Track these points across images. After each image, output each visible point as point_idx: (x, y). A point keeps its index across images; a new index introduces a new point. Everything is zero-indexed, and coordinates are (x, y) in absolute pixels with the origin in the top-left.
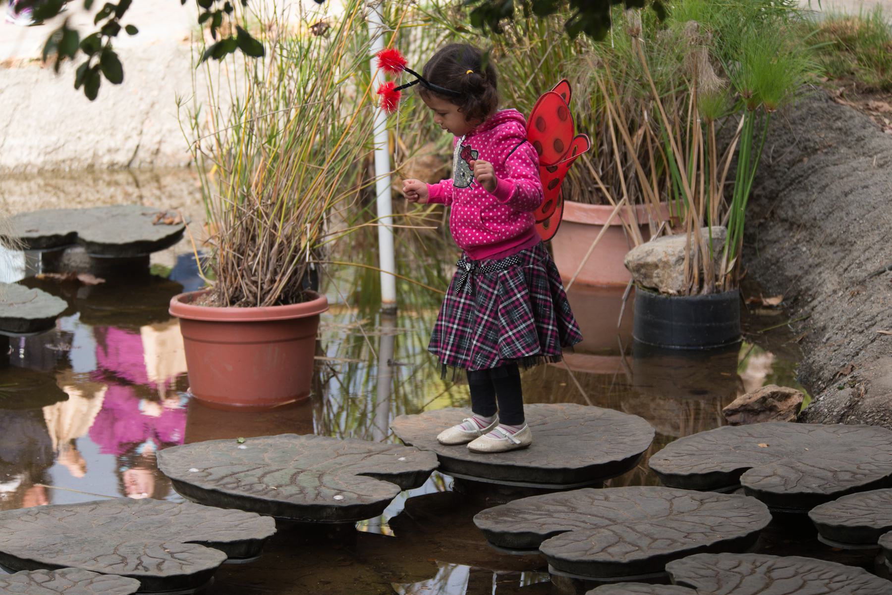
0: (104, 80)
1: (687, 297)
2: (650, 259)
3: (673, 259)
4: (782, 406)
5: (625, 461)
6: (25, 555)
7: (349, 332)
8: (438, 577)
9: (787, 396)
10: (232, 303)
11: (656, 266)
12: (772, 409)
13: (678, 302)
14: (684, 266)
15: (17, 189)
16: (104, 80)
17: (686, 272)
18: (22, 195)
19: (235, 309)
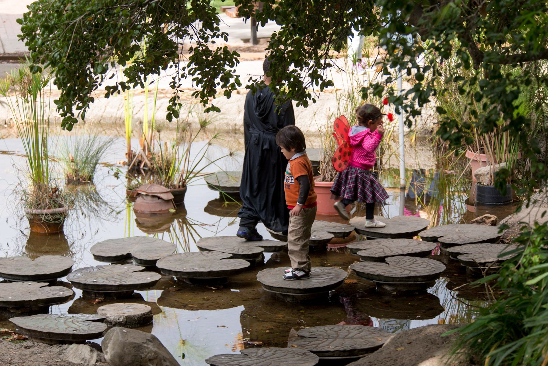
0: (173, 117)
1: (489, 186)
2: (479, 173)
3: (486, 173)
4: (487, 221)
5: (412, 233)
6: (204, 248)
7: (532, 224)
8: (488, 328)
9: (490, 218)
10: (323, 181)
11: (481, 175)
12: (484, 222)
13: (486, 188)
14: (489, 176)
15: (316, 140)
16: (173, 117)
17: (490, 178)
18: (318, 143)
19: (324, 183)
